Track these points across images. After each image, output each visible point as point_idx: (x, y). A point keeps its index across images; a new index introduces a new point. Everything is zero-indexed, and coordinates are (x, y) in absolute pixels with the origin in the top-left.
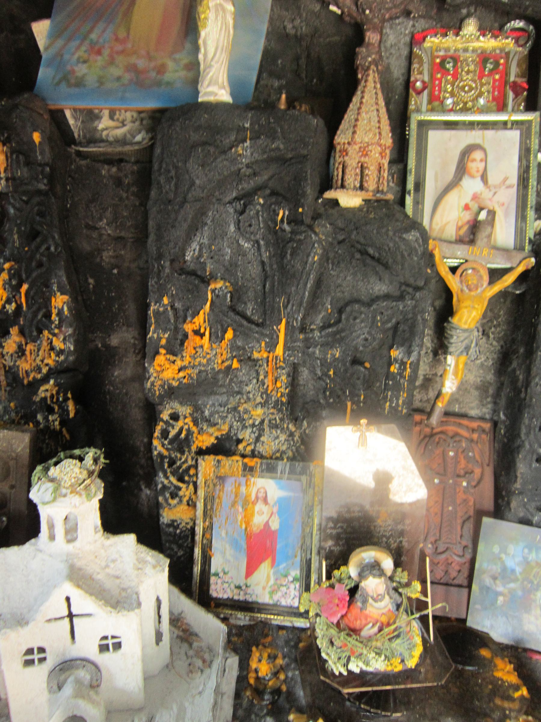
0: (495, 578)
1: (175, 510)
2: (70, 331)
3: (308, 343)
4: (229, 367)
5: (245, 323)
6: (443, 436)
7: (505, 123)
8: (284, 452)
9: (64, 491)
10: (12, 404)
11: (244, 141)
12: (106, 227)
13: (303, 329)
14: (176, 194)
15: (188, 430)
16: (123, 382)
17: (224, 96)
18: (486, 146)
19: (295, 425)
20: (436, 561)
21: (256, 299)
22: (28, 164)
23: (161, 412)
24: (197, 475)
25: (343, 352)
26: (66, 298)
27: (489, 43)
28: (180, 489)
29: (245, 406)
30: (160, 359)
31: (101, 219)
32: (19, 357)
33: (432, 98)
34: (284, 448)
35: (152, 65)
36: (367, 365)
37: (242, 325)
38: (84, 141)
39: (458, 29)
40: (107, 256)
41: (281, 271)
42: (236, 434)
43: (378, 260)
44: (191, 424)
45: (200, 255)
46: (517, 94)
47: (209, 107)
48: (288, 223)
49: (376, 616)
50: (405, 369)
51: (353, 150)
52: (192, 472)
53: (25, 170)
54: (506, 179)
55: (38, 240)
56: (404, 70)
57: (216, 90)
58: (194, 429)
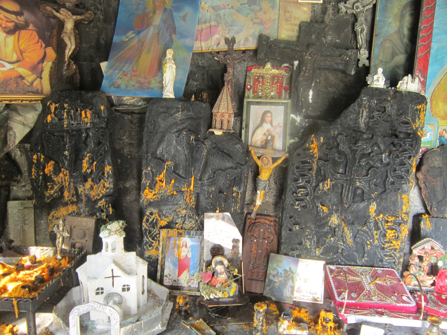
0: (274, 276)
1: (150, 252)
2: (112, 180)
3: (202, 185)
4: (173, 194)
5: (179, 177)
6: (259, 224)
7: (279, 103)
8: (194, 228)
9: (112, 233)
10: (87, 209)
11: (179, 112)
12: (126, 139)
13: (200, 180)
14: (154, 129)
15: (157, 219)
16: (131, 202)
17: (172, 96)
18: (272, 111)
19: (198, 217)
20: (253, 271)
21: (183, 168)
22: (99, 117)
23: (146, 212)
24: (159, 237)
25: (215, 188)
26: (110, 167)
27: (275, 71)
28: (153, 243)
29: (179, 209)
30: (146, 191)
31: (124, 136)
32: (91, 190)
33: (254, 92)
34: (194, 226)
35: (146, 81)
36: (225, 193)
37: (178, 178)
38: (117, 104)
39: (264, 66)
40: (126, 151)
41: (192, 159)
42: (175, 221)
43: (228, 155)
44: (158, 217)
45: (162, 152)
46: (286, 91)
47: (166, 100)
48: (195, 141)
49: (221, 281)
50: (239, 195)
51: (219, 115)
52: (158, 236)
53: (98, 120)
54: (279, 124)
55: (101, 145)
56: (244, 80)
57: (169, 93)
58: (159, 218)
